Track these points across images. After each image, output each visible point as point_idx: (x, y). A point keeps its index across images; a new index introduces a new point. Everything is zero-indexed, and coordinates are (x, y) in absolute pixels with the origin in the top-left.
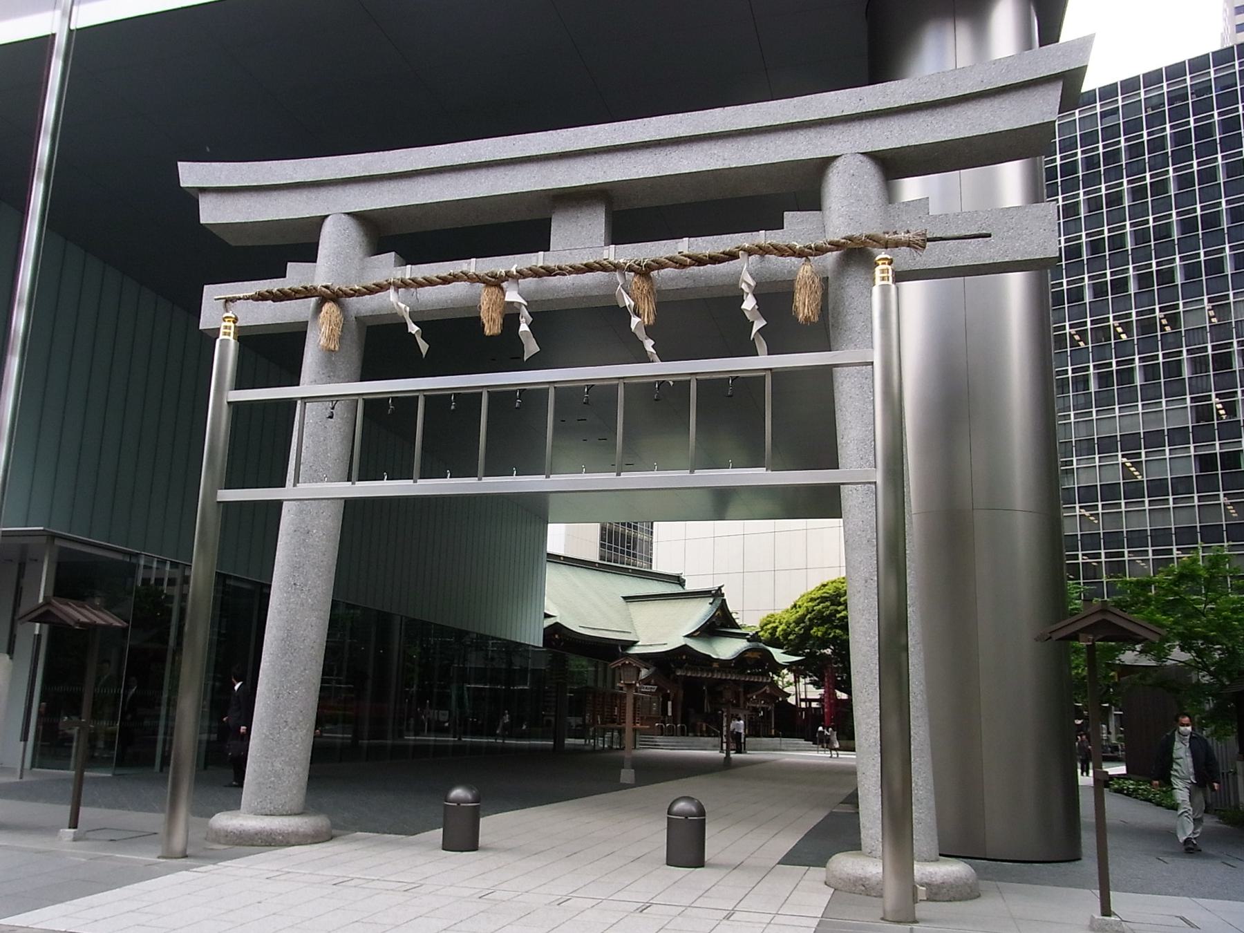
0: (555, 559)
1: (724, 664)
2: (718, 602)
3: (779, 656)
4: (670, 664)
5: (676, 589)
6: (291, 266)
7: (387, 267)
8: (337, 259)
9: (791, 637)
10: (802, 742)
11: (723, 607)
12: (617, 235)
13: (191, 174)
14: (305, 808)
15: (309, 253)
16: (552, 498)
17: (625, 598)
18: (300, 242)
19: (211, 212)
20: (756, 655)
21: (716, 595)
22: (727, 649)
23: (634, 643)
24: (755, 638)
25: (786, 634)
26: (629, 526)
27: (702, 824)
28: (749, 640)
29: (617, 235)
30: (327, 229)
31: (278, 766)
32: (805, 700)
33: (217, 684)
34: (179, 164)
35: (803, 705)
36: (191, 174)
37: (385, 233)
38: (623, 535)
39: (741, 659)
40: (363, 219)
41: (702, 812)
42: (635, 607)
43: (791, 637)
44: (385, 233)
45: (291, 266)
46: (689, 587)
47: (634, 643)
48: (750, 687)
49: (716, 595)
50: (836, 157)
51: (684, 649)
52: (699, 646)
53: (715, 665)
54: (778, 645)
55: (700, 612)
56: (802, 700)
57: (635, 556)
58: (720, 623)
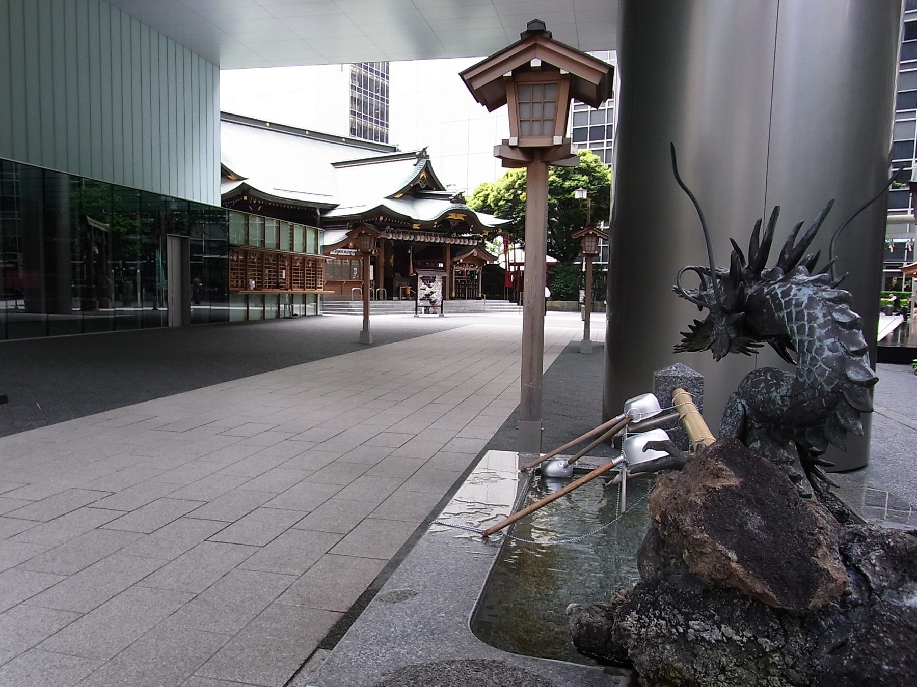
0: (227, 117)
1: (426, 227)
2: (423, 163)
3: (487, 220)
4: (371, 225)
9: (502, 203)
10: (507, 303)
11: (428, 169)
17: (333, 164)
20: (460, 217)
21: (422, 155)
22: (427, 211)
23: (334, 207)
24: (459, 199)
25: (497, 201)
26: (366, 68)
28: (452, 201)
32: (514, 264)
34: (219, 205)
35: (512, 269)
38: (371, 81)
39: (444, 224)
43: (502, 203)
47: (334, 207)
48: (457, 250)
49: (422, 155)
51: (381, 210)
52: (400, 208)
53: (415, 227)
54: (490, 212)
55: (406, 172)
56: (511, 264)
58: (424, 186)
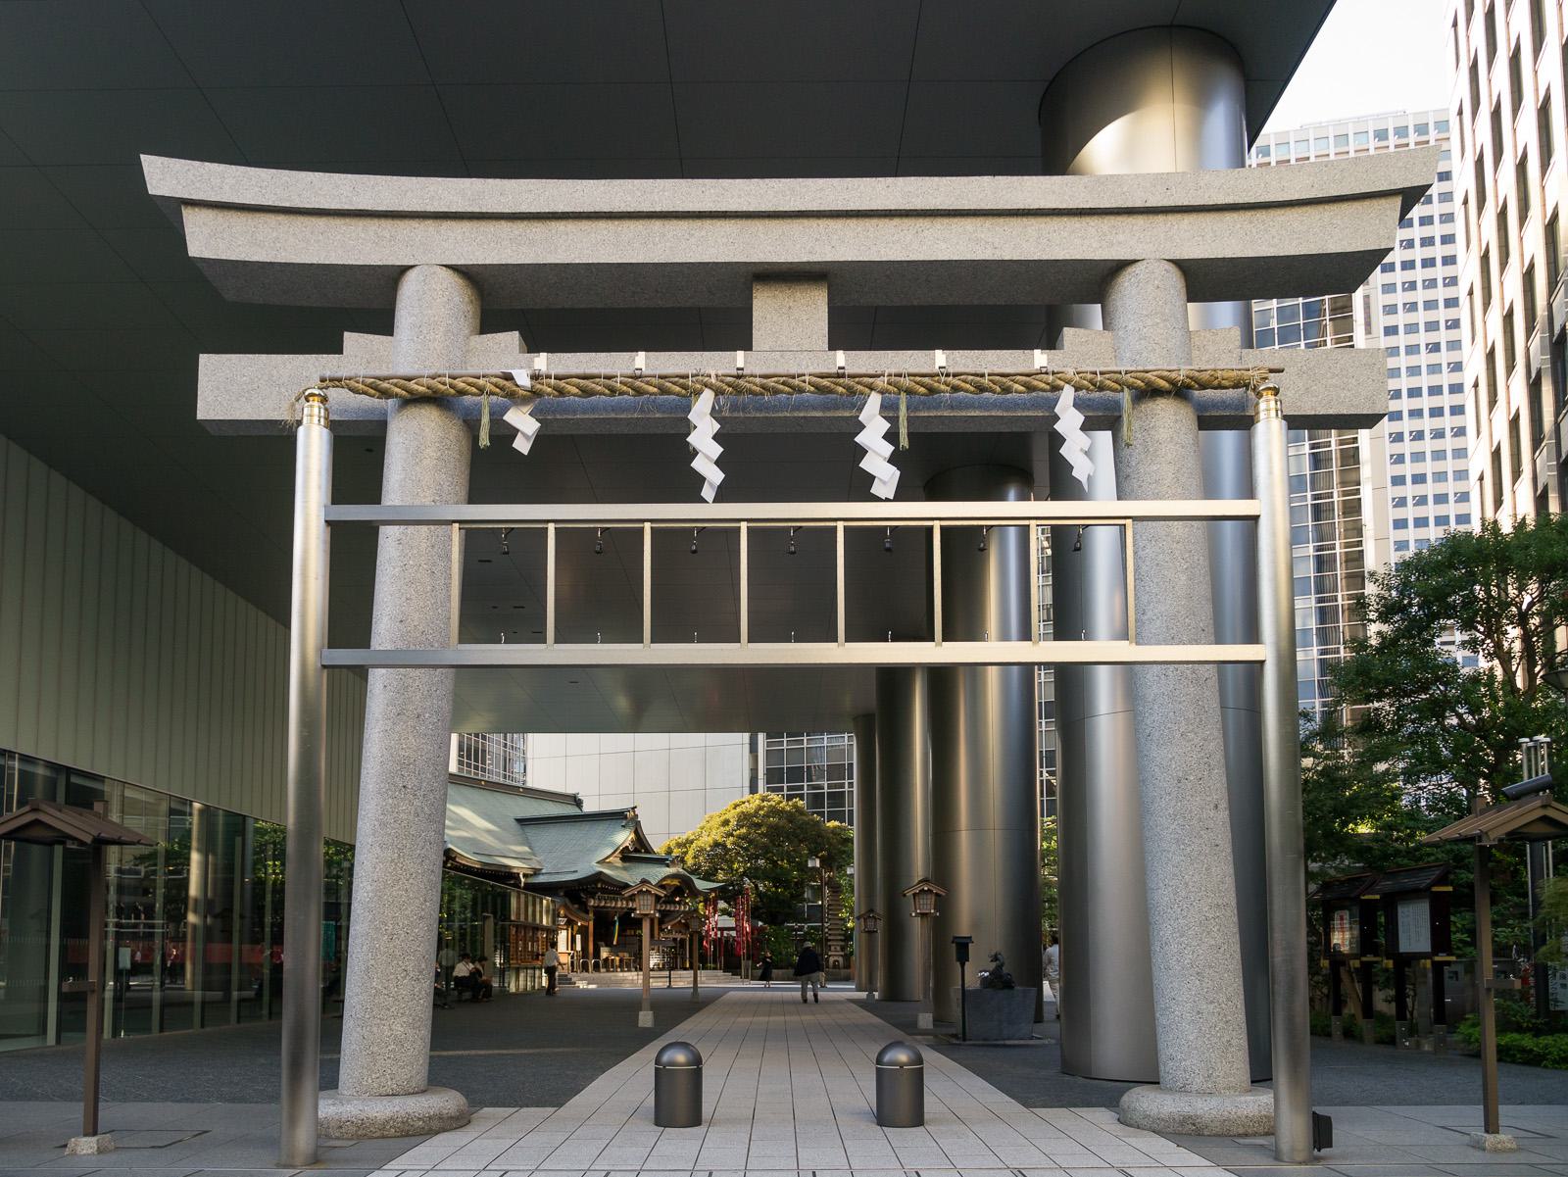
5: (572, 810)
6: (350, 338)
7: (505, 355)
8: (430, 336)
12: (841, 337)
13: (165, 176)
14: (423, 1084)
15: (381, 321)
16: (961, 673)
17: (521, 821)
18: (366, 301)
19: (206, 239)
27: (920, 1072)
29: (841, 337)
30: (409, 287)
31: (398, 1029)
33: (275, 929)
36: (165, 176)
37: (503, 300)
40: (470, 275)
41: (697, 1061)
42: (532, 832)
44: (503, 300)
45: (350, 338)
46: (589, 807)
50: (1135, 261)
57: (483, 770)
58: (638, 852)
